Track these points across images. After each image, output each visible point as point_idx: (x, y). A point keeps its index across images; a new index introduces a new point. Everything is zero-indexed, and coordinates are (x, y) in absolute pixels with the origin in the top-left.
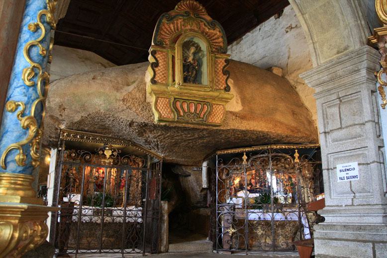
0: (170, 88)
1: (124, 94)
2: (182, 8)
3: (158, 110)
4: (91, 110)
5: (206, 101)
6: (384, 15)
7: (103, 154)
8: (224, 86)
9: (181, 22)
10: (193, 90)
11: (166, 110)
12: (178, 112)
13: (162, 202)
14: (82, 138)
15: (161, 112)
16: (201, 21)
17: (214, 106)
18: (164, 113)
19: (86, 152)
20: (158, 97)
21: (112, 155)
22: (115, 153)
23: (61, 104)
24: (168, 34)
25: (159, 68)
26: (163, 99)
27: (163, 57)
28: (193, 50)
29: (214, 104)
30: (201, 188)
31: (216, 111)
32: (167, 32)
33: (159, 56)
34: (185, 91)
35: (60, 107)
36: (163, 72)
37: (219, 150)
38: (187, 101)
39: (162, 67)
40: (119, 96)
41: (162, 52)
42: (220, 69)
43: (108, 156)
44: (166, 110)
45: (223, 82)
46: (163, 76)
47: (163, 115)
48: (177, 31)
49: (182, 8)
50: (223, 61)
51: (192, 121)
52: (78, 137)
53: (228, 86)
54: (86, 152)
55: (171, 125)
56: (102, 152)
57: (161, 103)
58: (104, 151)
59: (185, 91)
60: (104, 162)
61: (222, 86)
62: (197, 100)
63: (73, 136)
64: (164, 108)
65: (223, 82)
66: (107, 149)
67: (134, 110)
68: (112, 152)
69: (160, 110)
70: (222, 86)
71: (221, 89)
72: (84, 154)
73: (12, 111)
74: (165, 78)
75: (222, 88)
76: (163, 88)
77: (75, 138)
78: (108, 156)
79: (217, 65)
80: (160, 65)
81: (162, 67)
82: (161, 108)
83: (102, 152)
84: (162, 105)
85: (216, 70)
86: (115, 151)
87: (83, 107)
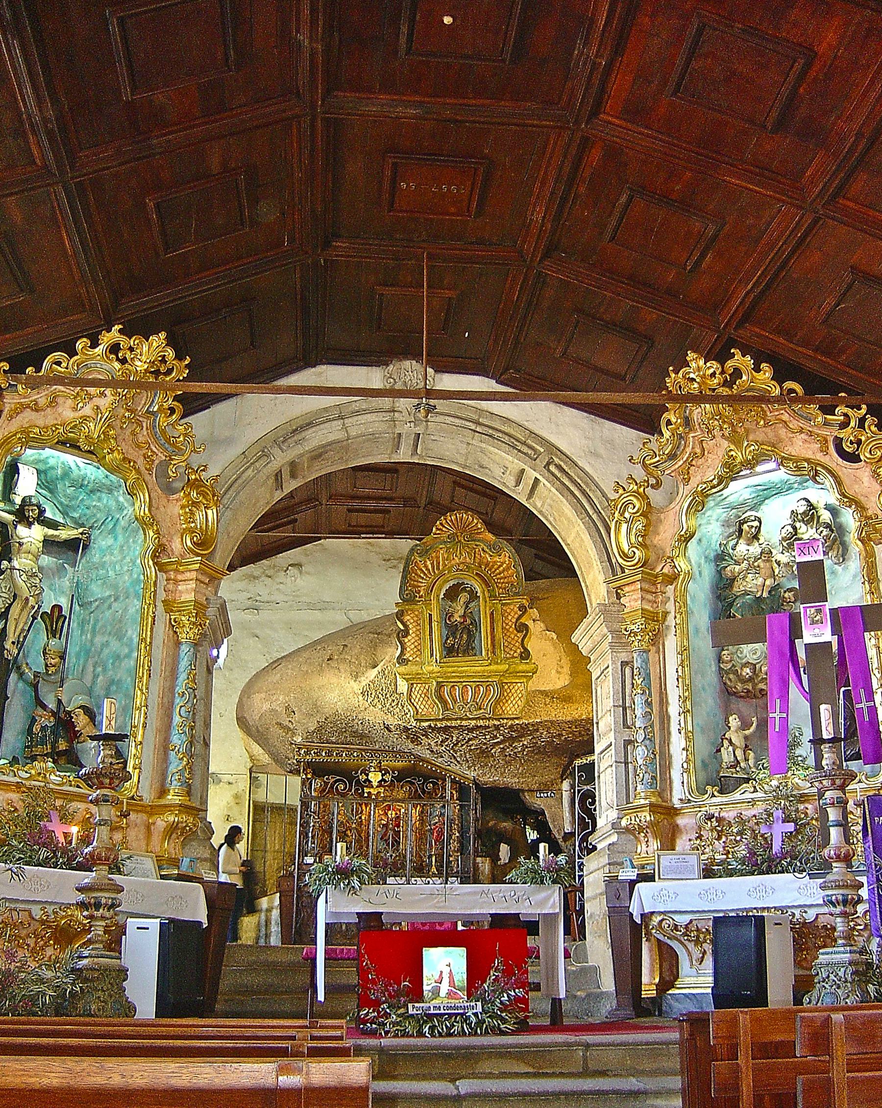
0: (427, 669)
1: (364, 684)
2: (444, 529)
3: (413, 704)
4: (328, 711)
5: (490, 680)
6: (621, 557)
7: (367, 780)
8: (518, 651)
9: (443, 554)
10: (463, 666)
11: (424, 703)
12: (444, 702)
13: (479, 860)
14: (329, 754)
15: (418, 707)
16: (476, 545)
17: (506, 687)
18: (422, 707)
19: (338, 778)
20: (412, 684)
21: (383, 780)
22: (388, 778)
23: (287, 705)
24: (423, 578)
25: (409, 638)
26: (419, 685)
27: (416, 619)
28: (463, 597)
29: (507, 683)
30: (562, 834)
31: (510, 695)
32: (422, 575)
33: (408, 617)
34: (450, 669)
35: (287, 708)
36: (416, 644)
37: (578, 756)
38: (458, 684)
39: (413, 635)
40: (357, 687)
41: (413, 611)
42: (510, 624)
43: (375, 784)
44: (424, 703)
45: (517, 644)
46: (415, 650)
47: (420, 710)
48: (436, 572)
49: (444, 529)
50: (516, 609)
51: (466, 715)
52: (324, 754)
53: (526, 649)
54: (338, 778)
55: (439, 725)
56: (365, 777)
57: (416, 693)
58: (367, 775)
59: (450, 669)
60: (369, 793)
61: (515, 652)
62: (474, 680)
63: (314, 753)
64: (421, 699)
65: (517, 644)
66: (373, 770)
67: (380, 707)
68: (383, 775)
69: (415, 704)
70: (515, 652)
71: (513, 657)
72: (335, 782)
73: (173, 750)
74: (418, 653)
75: (515, 655)
76: (414, 669)
77: (318, 756)
78: (375, 784)
79: (507, 618)
80: (411, 632)
81: (413, 635)
82: (417, 700)
83: (365, 777)
84: (419, 696)
85: (673, 564)
86: (387, 772)
87: (316, 707)
